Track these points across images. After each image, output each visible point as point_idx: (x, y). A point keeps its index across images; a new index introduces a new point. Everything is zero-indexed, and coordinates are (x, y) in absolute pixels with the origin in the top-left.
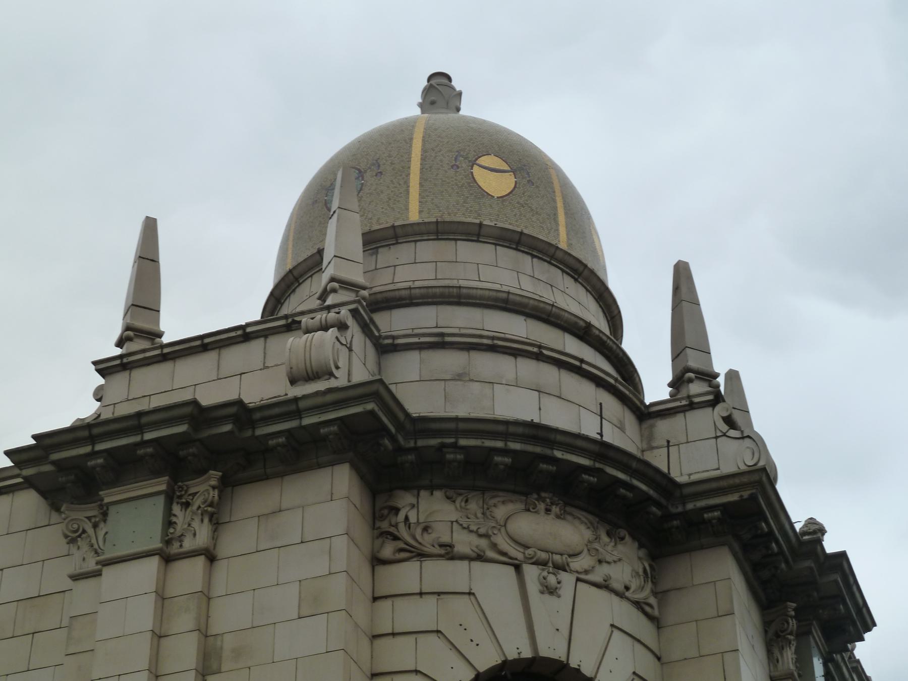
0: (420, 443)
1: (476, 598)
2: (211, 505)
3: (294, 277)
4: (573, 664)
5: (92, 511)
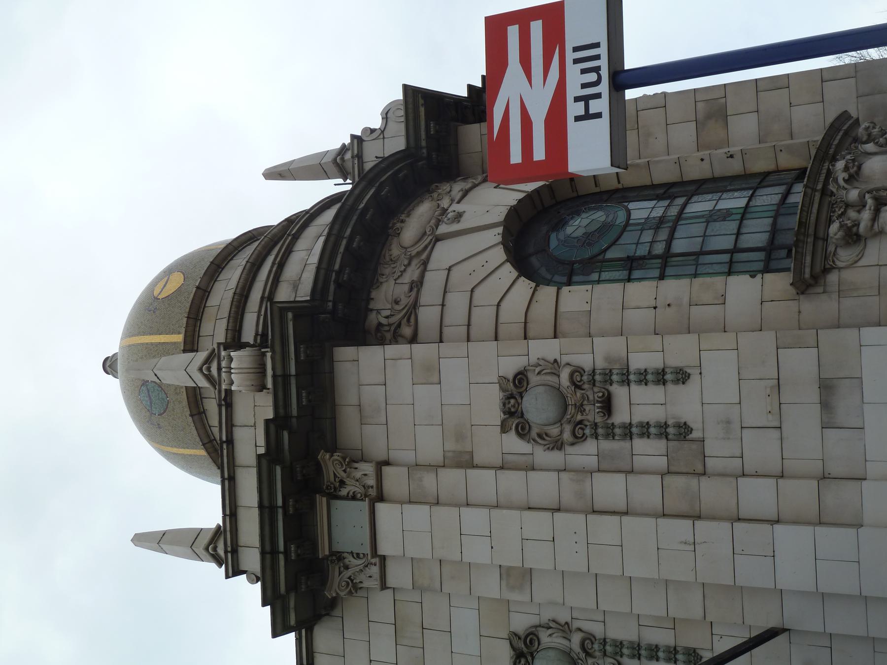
0: (331, 298)
2: (344, 459)
3: (209, 442)
5: (334, 570)
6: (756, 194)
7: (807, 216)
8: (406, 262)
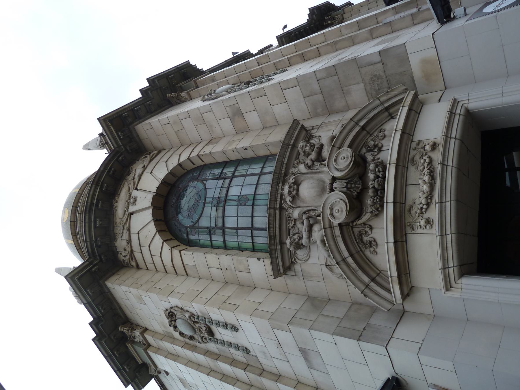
1: (139, 231)
4: (155, 190)
6: (266, 166)
8: (122, 228)
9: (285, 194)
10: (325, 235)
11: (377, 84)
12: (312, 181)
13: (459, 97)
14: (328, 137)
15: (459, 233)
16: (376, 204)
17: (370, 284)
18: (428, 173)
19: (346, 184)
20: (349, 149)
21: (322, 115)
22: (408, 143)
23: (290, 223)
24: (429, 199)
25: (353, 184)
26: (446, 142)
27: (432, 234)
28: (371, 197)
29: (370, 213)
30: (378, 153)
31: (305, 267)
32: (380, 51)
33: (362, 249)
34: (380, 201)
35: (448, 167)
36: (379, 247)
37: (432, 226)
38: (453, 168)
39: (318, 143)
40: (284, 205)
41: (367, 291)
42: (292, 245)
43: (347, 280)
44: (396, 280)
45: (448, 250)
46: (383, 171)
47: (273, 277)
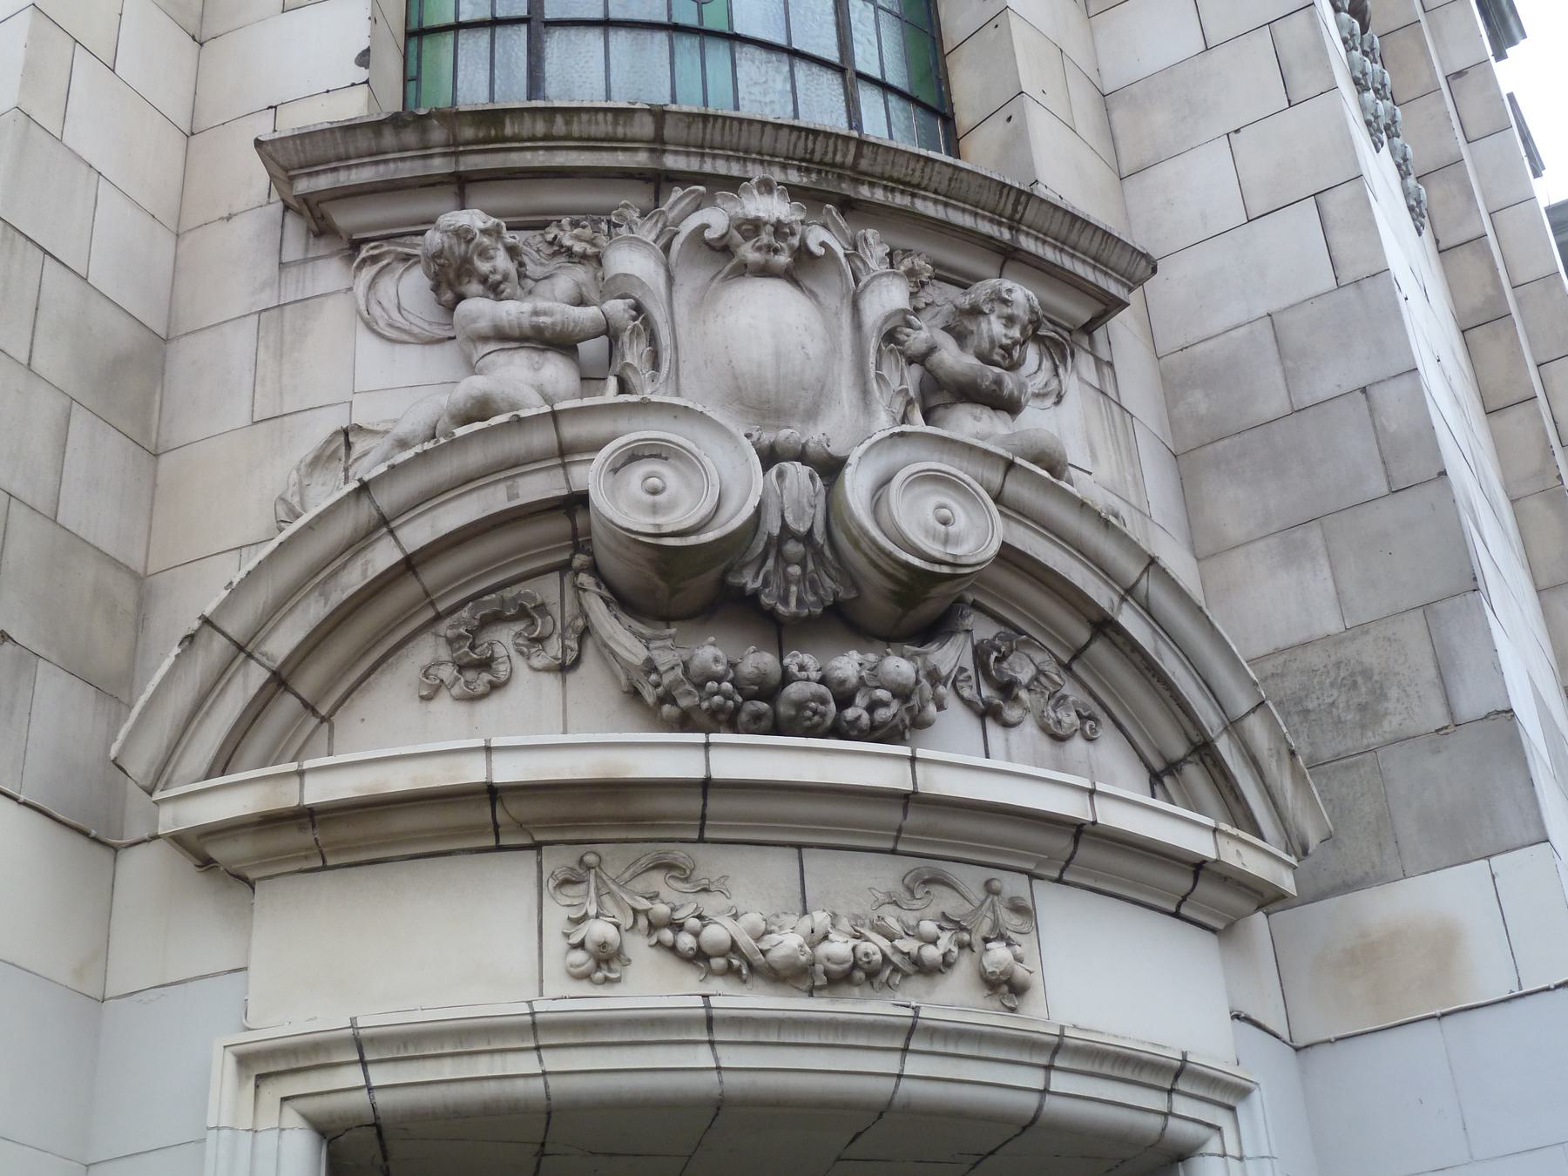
6: (893, 100)
7: (533, 139)
9: (744, 201)
10: (519, 421)
11: (1333, 703)
12: (815, 348)
13: (1259, 1117)
14: (1056, 434)
15: (549, 1114)
16: (696, 692)
17: (253, 663)
18: (867, 955)
19: (802, 529)
20: (995, 547)
21: (1170, 417)
22: (1028, 859)
23: (575, 232)
24: (730, 963)
25: (804, 567)
26: (1028, 1044)
27: (541, 981)
28: (732, 665)
29: (649, 661)
30: (968, 703)
31: (333, 319)
32: (1514, 715)
33: (448, 622)
34: (714, 713)
35: (897, 1057)
36: (462, 708)
37: (586, 976)
38: (892, 1082)
39: (1022, 386)
40: (681, 198)
41: (217, 646)
42: (455, 241)
43: (274, 544)
44: (286, 797)
45: (457, 1060)
46: (874, 727)
47: (266, 135)
